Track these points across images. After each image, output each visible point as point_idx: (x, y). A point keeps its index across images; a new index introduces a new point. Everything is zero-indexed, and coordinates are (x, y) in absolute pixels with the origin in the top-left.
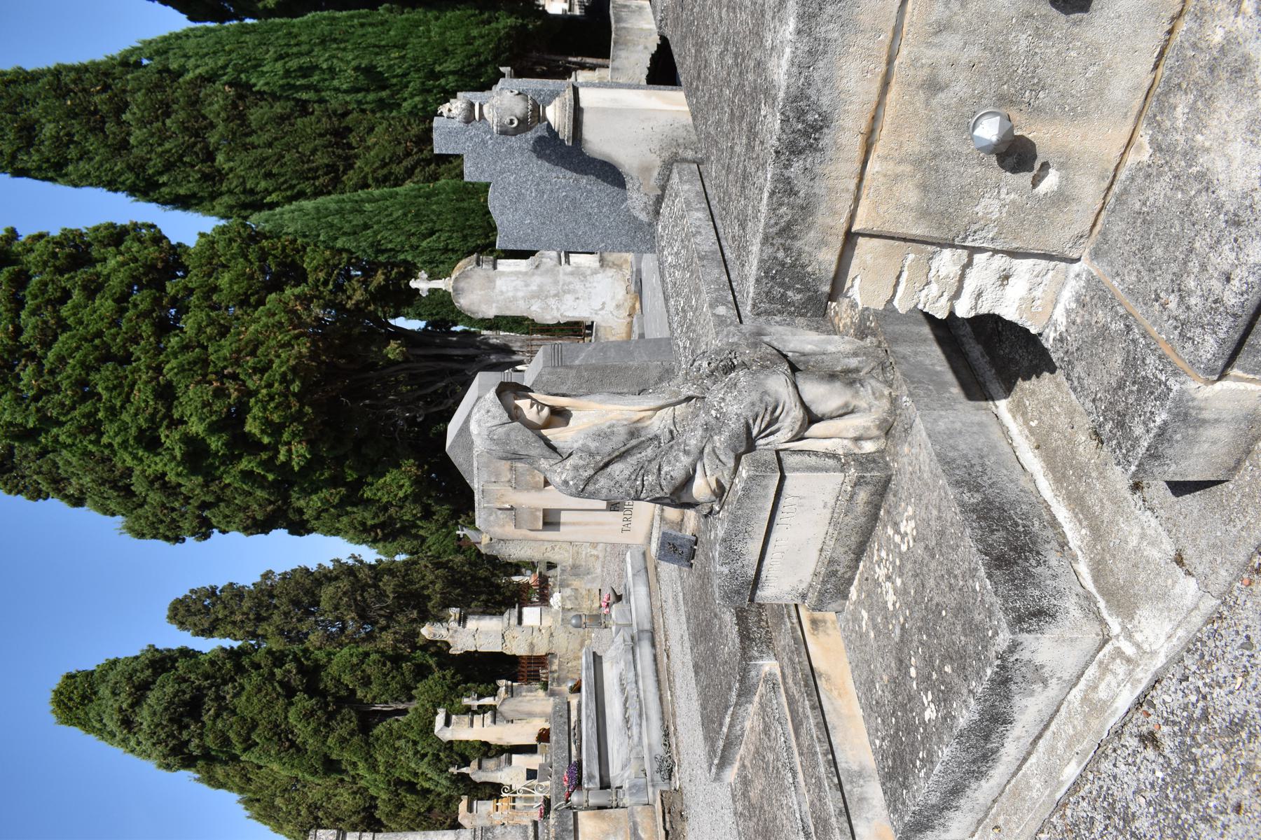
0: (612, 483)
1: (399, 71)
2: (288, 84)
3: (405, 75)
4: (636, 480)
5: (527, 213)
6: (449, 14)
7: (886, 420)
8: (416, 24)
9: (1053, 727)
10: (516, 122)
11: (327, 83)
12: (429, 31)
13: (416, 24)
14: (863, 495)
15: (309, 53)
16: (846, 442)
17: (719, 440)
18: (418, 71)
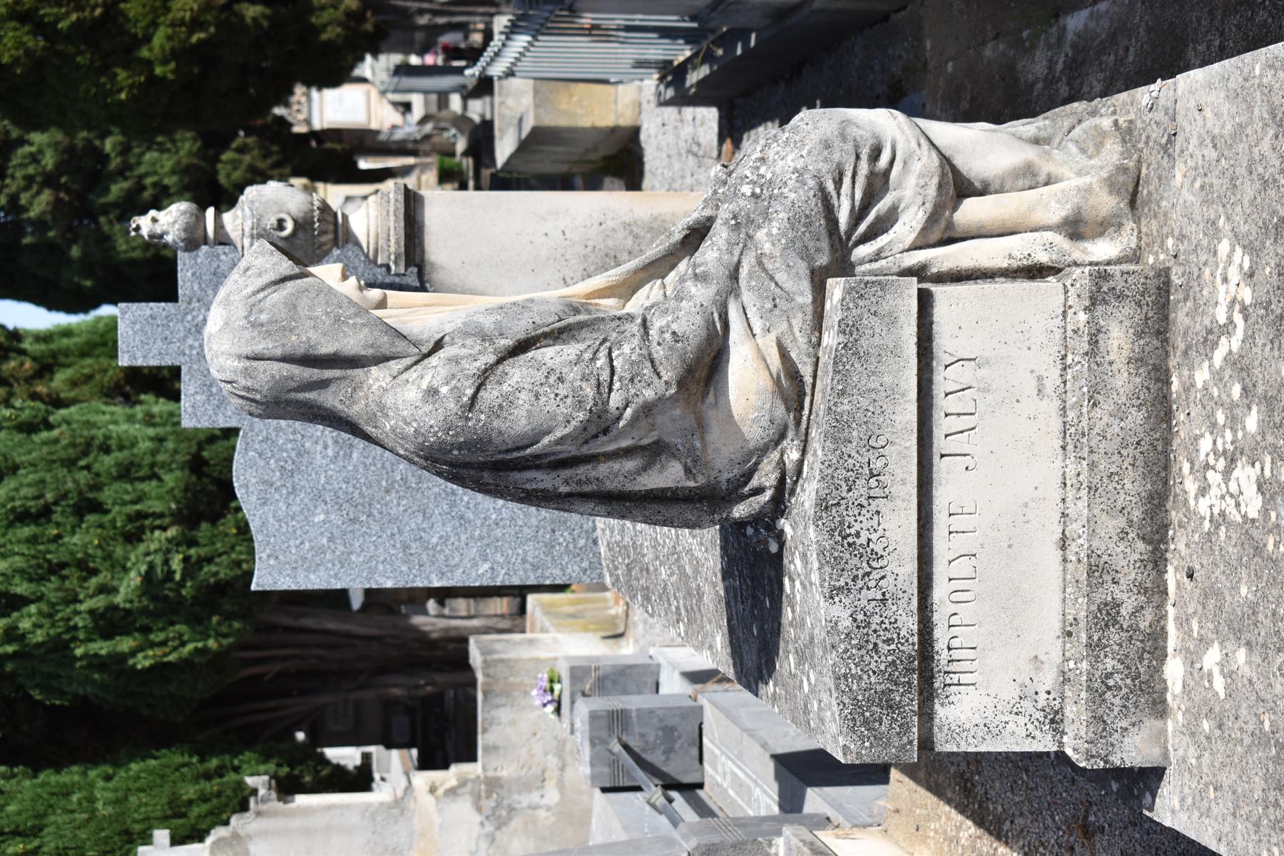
0: (540, 376)
4: (594, 359)
5: (318, 497)
6: (134, 767)
7: (1122, 169)
8: (66, 793)
10: (289, 226)
12: (91, 800)
13: (66, 793)
14: (1119, 338)
16: (1049, 236)
17: (767, 238)
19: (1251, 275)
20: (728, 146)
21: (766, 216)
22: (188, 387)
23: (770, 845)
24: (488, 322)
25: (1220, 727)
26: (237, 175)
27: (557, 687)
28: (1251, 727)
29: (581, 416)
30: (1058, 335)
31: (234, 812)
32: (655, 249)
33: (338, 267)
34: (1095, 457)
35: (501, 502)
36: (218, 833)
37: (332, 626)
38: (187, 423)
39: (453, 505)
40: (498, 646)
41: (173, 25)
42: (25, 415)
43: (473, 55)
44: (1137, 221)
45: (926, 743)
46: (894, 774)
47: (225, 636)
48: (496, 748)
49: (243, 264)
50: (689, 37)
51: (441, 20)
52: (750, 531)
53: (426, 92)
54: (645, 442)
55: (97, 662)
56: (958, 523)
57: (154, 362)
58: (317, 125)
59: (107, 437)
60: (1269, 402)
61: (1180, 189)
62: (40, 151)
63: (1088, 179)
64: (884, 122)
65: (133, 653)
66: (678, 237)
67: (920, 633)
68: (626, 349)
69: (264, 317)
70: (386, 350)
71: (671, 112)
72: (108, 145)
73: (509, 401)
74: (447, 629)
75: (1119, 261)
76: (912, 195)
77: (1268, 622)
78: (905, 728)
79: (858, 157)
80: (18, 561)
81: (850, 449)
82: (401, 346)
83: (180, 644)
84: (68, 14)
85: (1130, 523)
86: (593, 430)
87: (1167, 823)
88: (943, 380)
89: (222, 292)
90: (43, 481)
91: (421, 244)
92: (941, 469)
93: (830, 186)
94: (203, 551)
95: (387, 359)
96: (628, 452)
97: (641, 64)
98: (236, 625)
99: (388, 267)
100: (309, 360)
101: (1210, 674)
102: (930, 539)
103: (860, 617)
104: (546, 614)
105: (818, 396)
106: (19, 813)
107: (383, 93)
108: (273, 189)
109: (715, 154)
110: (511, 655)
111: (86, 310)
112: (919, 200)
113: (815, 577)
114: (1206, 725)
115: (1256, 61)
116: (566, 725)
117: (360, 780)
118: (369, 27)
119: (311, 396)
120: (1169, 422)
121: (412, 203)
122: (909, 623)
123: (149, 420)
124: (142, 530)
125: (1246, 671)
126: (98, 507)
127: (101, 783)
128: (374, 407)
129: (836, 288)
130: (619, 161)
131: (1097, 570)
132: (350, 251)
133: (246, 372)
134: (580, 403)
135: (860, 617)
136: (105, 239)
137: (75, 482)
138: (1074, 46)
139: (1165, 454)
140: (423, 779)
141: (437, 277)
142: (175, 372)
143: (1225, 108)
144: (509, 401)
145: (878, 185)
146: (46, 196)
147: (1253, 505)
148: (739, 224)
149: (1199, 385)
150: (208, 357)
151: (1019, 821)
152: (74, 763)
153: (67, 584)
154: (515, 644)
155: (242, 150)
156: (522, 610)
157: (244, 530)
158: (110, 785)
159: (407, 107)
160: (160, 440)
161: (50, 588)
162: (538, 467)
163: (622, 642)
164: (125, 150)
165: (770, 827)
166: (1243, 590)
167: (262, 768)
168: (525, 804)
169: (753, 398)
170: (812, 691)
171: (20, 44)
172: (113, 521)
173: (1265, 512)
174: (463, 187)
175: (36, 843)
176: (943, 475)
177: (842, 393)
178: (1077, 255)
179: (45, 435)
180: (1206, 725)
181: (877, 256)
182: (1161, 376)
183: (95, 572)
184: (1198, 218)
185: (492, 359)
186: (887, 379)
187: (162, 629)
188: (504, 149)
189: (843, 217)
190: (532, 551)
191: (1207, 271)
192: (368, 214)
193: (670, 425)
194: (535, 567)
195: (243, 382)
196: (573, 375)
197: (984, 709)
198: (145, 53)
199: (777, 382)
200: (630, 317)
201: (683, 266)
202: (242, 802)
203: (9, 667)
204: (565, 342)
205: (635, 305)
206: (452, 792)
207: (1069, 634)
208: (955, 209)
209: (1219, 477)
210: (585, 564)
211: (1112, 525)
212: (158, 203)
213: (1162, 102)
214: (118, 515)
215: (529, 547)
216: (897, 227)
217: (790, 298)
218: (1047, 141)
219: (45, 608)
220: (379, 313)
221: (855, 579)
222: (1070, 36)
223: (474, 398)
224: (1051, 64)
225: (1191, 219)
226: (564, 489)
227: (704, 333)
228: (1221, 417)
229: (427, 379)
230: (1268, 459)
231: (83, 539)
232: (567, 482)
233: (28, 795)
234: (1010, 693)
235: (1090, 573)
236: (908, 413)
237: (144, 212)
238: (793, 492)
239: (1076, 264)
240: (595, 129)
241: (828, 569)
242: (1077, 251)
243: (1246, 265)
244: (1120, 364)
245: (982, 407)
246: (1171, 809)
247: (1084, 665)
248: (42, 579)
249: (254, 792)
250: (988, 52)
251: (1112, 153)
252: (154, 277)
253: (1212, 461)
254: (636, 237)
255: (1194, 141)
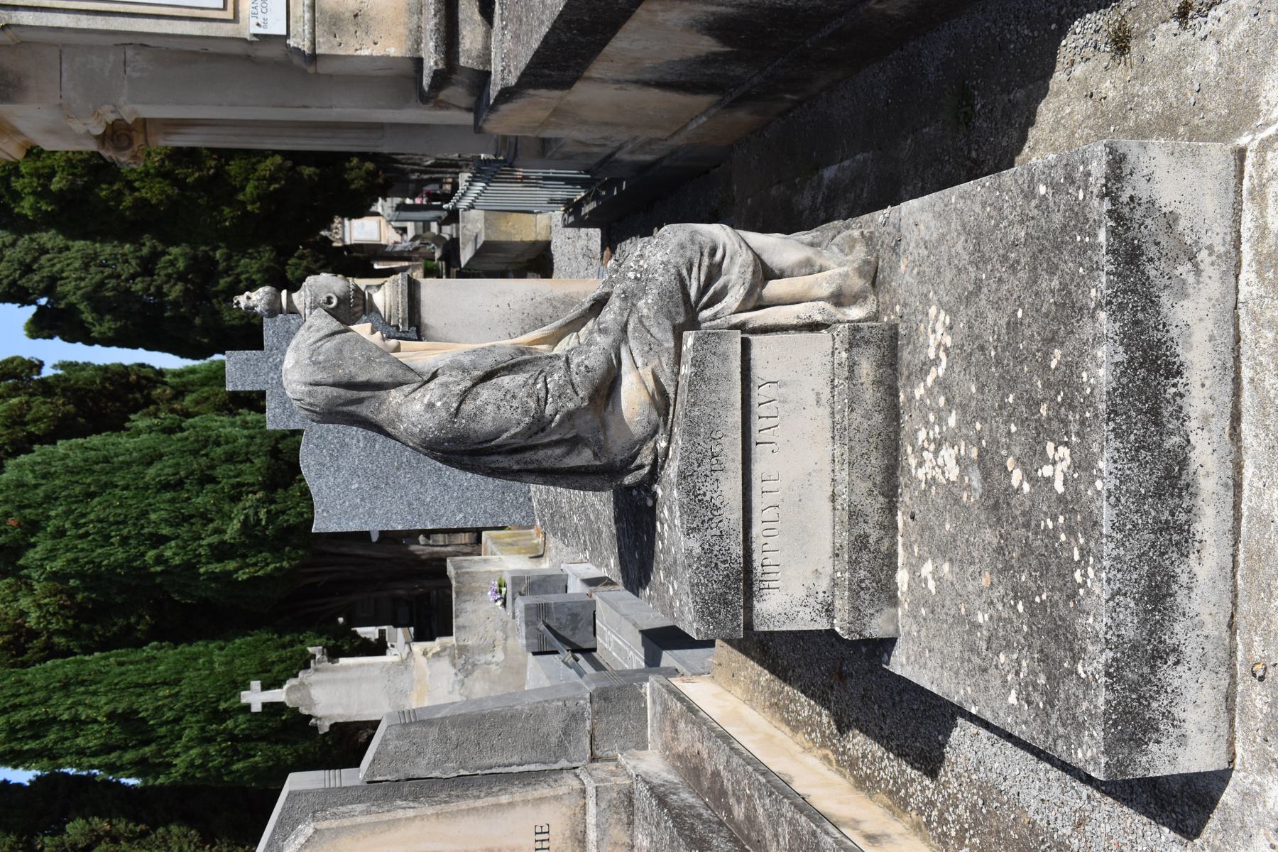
0: (500, 395)
1: (169, 715)
2: (12, 751)
3: (177, 720)
4: (535, 383)
5: (354, 473)
6: (237, 641)
7: (867, 262)
8: (195, 658)
9: (1246, 373)
10: (335, 301)
11: (67, 744)
12: (211, 662)
13: (195, 658)
14: (866, 369)
15: (44, 702)
16: (821, 303)
17: (645, 305)
18: (196, 712)
19: (951, 328)
20: (607, 252)
21: (644, 292)
22: (270, 404)
23: (641, 687)
24: (466, 360)
25: (932, 612)
26: (298, 273)
27: (504, 590)
28: (952, 612)
29: (527, 420)
30: (829, 367)
31: (301, 669)
32: (573, 313)
33: (369, 325)
34: (853, 444)
35: (470, 475)
36: (291, 682)
37: (360, 552)
38: (270, 426)
39: (439, 477)
40: (465, 564)
41: (258, 179)
42: (167, 423)
43: (447, 198)
44: (876, 295)
45: (749, 625)
46: (718, 642)
47: (293, 559)
48: (464, 627)
49: (307, 324)
50: (584, 184)
51: (426, 177)
52: (635, 493)
53: (415, 221)
54: (568, 436)
55: (213, 576)
56: (767, 486)
57: (248, 388)
58: (348, 242)
59: (219, 436)
60: (963, 408)
61: (904, 274)
62: (176, 259)
63: (845, 269)
64: (718, 232)
65: (236, 571)
66: (587, 305)
67: (744, 556)
68: (556, 377)
69: (321, 358)
70: (401, 379)
71: (571, 232)
72: (218, 254)
73: (481, 410)
74: (432, 553)
75: (865, 320)
76: (736, 278)
77: (963, 546)
78: (735, 616)
79: (702, 254)
80: (163, 514)
81: (699, 439)
82: (410, 376)
83: (265, 565)
84: (193, 173)
85: (875, 484)
86: (535, 429)
87: (898, 673)
88: (758, 395)
89: (293, 342)
90: (178, 464)
91: (419, 312)
92: (757, 451)
93: (685, 273)
94: (279, 507)
95: (401, 384)
96: (557, 443)
97: (552, 201)
98: (301, 552)
99: (398, 327)
100: (351, 385)
101: (926, 579)
102: (750, 496)
103: (706, 547)
104: (495, 543)
105: (678, 406)
106: (166, 671)
107: (389, 222)
108: (325, 278)
109: (599, 256)
110: (474, 569)
111: (205, 358)
112: (741, 281)
113: (677, 522)
114: (923, 611)
115: (952, 194)
116: (509, 613)
117: (379, 648)
118: (381, 181)
119: (352, 408)
120: (898, 421)
121: (413, 290)
122: (738, 550)
123: (245, 425)
124: (241, 494)
125: (950, 577)
126: (213, 480)
127: (217, 652)
128: (393, 415)
129: (689, 338)
130: (537, 261)
131: (855, 515)
132: (373, 316)
133: (310, 394)
134: (526, 412)
135: (706, 547)
136: (216, 313)
137: (199, 464)
138: (828, 188)
139: (896, 440)
140: (418, 647)
141: (429, 333)
142: (262, 395)
143: (932, 224)
144: (481, 410)
145: (715, 271)
146: (179, 287)
147: (953, 473)
148: (627, 297)
149: (918, 397)
150: (285, 384)
151: (798, 670)
152: (200, 639)
153: (194, 528)
154: (476, 562)
155: (301, 257)
156: (479, 540)
157: (306, 493)
158: (223, 653)
159: (404, 230)
160: (252, 437)
161: (184, 530)
162: (499, 453)
163: (542, 560)
164: (228, 258)
165: (641, 676)
166: (948, 527)
167: (317, 641)
168: (483, 661)
169: (637, 407)
170: (676, 593)
171: (163, 192)
172: (223, 488)
173: (961, 477)
174: (440, 277)
175: (177, 689)
176: (758, 455)
177: (694, 404)
178: (839, 316)
179: (179, 435)
180: (923, 611)
181: (715, 317)
182: (893, 392)
183: (212, 520)
184: (916, 292)
185: (469, 384)
186: (722, 395)
187: (254, 556)
188: (466, 255)
189: (693, 292)
190: (490, 506)
191: (922, 326)
192: (385, 295)
193: (584, 426)
194: (492, 516)
195: (308, 400)
196: (522, 394)
197: (787, 602)
198: (241, 197)
199: (652, 397)
200: (558, 357)
201: (590, 324)
202: (305, 662)
203: (158, 580)
204: (516, 373)
205: (561, 348)
206: (437, 655)
207: (837, 555)
208: (763, 287)
209: (931, 456)
210: (524, 513)
211: (863, 486)
212: (252, 286)
213: (891, 220)
214: (225, 484)
215: (488, 503)
216: (727, 299)
217: (660, 345)
218: (819, 245)
219: (181, 543)
220: (395, 355)
221: (703, 522)
222: (826, 182)
223: (458, 409)
224: (814, 198)
225: (911, 294)
226: (515, 467)
227: (605, 366)
228: (932, 418)
229: (428, 397)
230: (963, 444)
231: (203, 500)
232: (518, 463)
233: (171, 660)
234: (800, 593)
235: (850, 517)
236: (736, 416)
237: (242, 293)
238: (662, 468)
239: (839, 322)
240: (523, 243)
241: (686, 516)
242: (839, 314)
243: (948, 322)
244: (868, 385)
245: (782, 413)
246: (900, 664)
247: (847, 575)
248: (178, 525)
249: (314, 656)
250: (773, 192)
251: (860, 252)
252: (248, 334)
253: (926, 445)
254: (555, 307)
255: (913, 244)
